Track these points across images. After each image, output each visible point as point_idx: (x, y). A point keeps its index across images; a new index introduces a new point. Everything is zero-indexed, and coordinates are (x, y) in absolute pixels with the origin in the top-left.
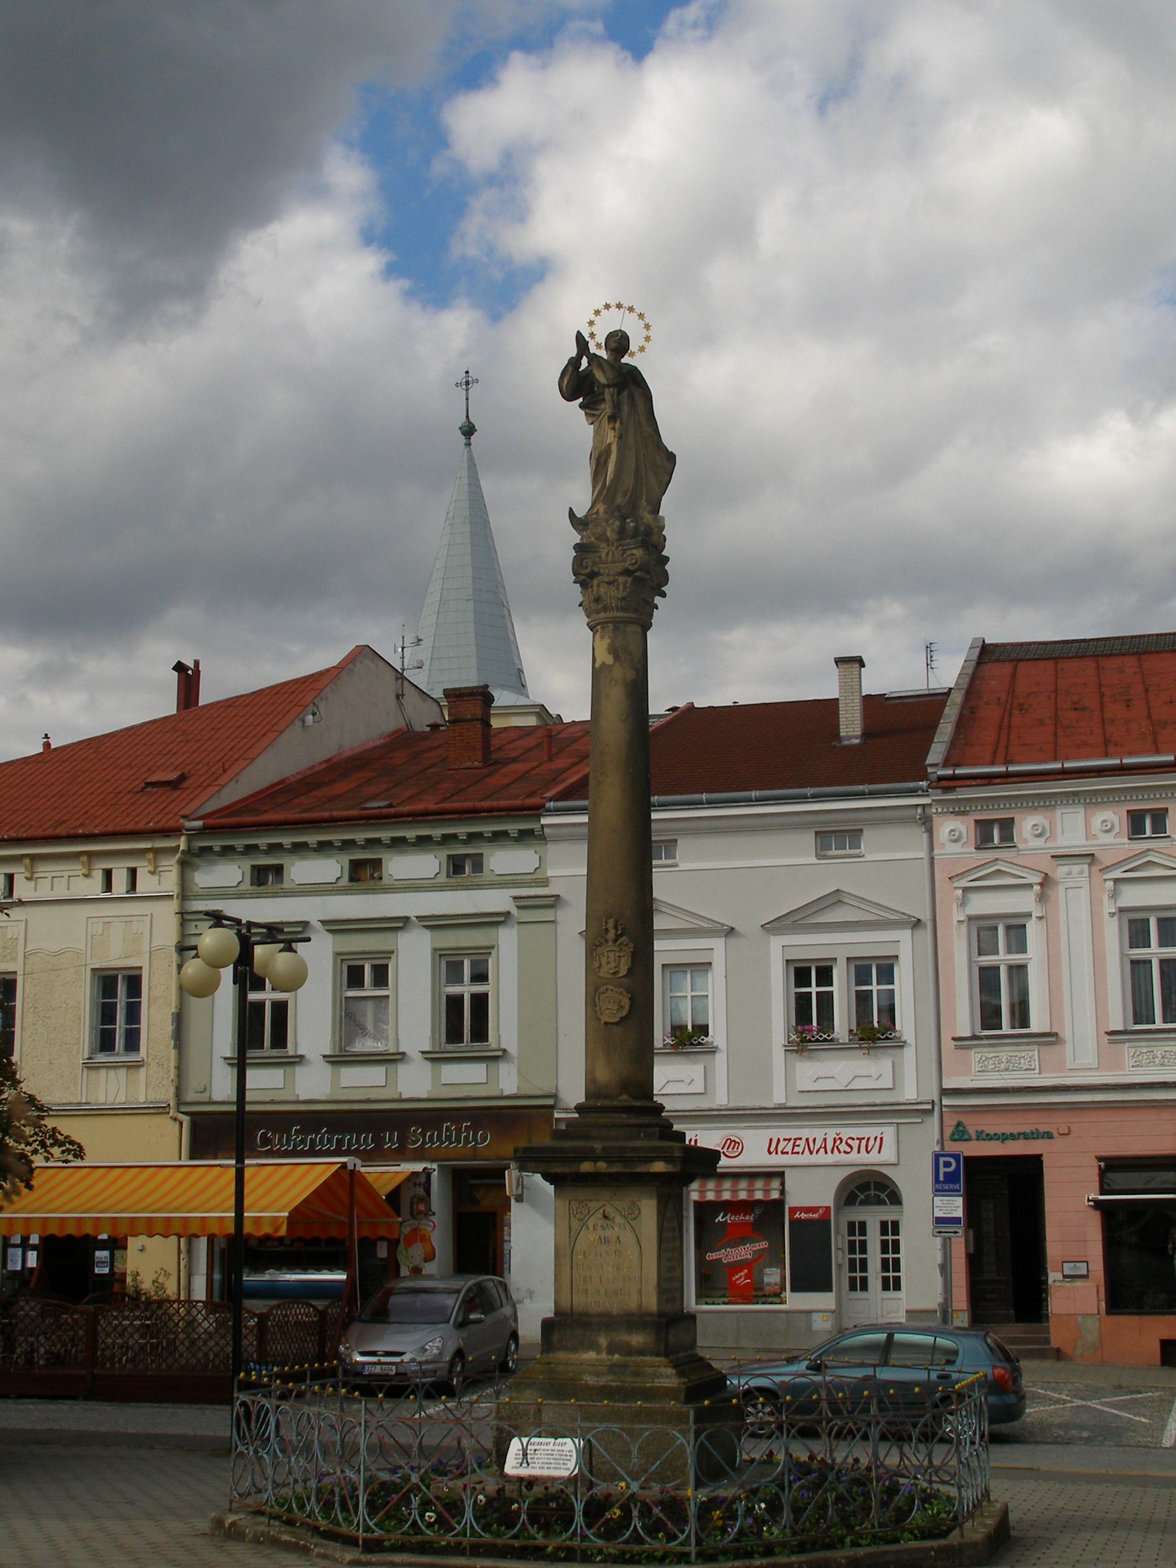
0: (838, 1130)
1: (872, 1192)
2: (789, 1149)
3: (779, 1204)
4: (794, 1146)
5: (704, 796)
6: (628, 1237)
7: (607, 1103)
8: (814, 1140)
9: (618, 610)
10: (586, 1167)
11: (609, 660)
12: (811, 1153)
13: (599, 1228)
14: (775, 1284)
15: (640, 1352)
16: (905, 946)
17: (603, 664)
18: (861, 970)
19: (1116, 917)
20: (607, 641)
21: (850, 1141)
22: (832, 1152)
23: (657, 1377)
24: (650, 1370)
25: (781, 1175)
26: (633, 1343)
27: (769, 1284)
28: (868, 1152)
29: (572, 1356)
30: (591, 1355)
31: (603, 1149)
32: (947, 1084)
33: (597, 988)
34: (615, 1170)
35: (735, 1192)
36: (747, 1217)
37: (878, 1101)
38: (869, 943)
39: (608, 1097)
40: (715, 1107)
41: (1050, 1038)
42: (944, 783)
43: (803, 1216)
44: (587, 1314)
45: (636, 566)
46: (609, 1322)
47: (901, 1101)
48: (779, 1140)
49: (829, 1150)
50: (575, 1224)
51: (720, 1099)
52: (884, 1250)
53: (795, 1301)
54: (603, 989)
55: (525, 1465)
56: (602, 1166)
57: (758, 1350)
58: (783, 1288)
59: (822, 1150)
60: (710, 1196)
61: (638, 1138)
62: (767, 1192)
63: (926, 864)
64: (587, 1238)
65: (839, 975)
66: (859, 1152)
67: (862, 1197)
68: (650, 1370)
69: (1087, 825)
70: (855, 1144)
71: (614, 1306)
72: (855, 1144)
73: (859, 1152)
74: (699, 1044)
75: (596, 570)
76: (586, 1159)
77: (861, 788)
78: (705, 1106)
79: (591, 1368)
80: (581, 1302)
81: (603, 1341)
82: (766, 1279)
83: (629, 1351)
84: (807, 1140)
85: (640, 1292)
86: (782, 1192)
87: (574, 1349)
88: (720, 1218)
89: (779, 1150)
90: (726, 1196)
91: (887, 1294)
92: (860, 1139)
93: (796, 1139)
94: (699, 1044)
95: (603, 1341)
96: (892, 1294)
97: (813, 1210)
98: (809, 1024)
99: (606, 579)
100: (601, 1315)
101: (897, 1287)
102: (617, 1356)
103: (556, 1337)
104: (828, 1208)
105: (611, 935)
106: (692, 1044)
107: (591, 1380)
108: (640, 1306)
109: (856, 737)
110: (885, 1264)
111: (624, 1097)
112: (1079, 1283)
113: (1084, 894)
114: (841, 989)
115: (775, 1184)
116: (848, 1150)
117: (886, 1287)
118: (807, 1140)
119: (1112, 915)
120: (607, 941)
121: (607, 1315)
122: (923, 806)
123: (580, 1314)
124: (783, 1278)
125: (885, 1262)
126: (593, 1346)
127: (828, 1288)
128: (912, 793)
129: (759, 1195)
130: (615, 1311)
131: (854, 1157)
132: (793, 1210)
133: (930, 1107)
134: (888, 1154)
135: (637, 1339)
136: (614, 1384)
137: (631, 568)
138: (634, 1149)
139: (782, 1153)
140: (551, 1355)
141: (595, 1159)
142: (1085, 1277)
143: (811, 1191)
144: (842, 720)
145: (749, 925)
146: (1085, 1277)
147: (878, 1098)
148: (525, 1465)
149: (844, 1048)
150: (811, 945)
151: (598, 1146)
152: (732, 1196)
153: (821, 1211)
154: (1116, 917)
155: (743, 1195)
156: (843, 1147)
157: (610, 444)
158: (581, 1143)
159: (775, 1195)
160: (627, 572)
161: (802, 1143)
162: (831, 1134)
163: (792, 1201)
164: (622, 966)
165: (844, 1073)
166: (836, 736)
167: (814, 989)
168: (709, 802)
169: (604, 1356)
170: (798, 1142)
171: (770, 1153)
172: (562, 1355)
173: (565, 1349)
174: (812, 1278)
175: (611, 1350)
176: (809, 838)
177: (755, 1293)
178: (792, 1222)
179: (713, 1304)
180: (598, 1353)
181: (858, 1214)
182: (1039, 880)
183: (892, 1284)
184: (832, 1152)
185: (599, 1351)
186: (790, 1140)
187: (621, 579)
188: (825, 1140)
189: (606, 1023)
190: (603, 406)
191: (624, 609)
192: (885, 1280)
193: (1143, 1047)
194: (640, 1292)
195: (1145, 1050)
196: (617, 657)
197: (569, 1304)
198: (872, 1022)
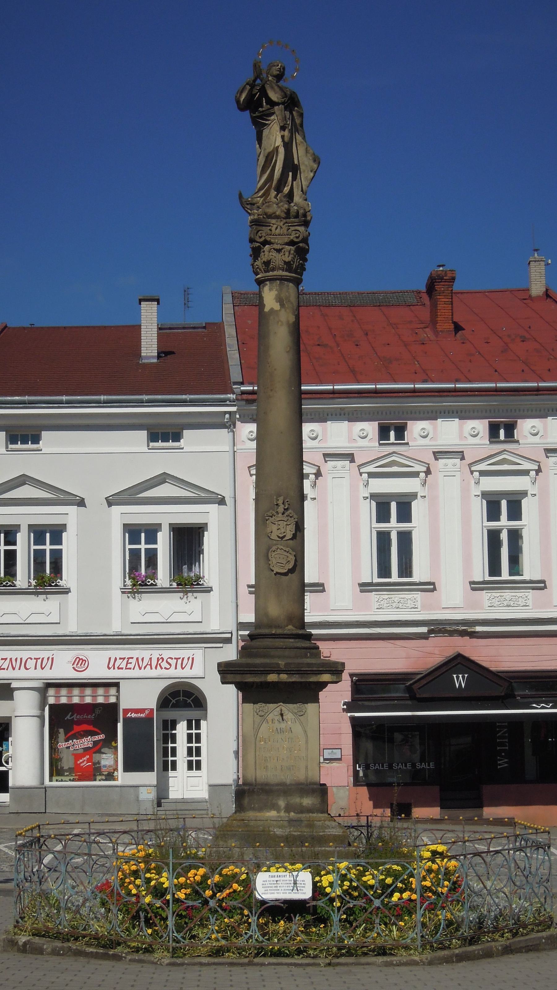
0: (160, 652)
1: (181, 698)
2: (123, 665)
3: (115, 707)
4: (127, 663)
5: (64, 398)
6: (297, 728)
7: (279, 631)
8: (143, 659)
9: (283, 270)
10: (272, 678)
11: (277, 307)
12: (140, 668)
13: (276, 722)
14: (110, 766)
15: (310, 810)
16: (210, 515)
17: (272, 309)
18: (38, 533)
19: (368, 500)
20: (274, 293)
21: (169, 660)
22: (156, 668)
23: (326, 828)
24: (320, 823)
25: (117, 685)
26: (304, 804)
27: (105, 766)
28: (183, 668)
29: (259, 815)
30: (273, 813)
31: (286, 664)
32: (241, 620)
33: (269, 548)
34: (294, 680)
35: (70, 697)
36: (89, 717)
37: (191, 631)
38: (187, 515)
39: (278, 627)
40: (68, 634)
41: (430, 587)
42: (245, 397)
43: (133, 715)
44: (267, 784)
45: (300, 238)
46: (285, 789)
47: (208, 631)
48: (116, 659)
49: (153, 667)
50: (258, 719)
51: (72, 627)
52: (190, 740)
53: (123, 778)
54: (274, 548)
55: (295, 891)
56: (284, 677)
57: (103, 815)
58: (116, 769)
59: (149, 667)
60: (64, 700)
61: (306, 657)
62: (107, 697)
63: (228, 457)
64: (264, 729)
65: (21, 538)
66: (176, 668)
67: (174, 701)
68: (320, 823)
69: (350, 431)
70: (173, 662)
71: (288, 778)
72: (173, 662)
73: (176, 668)
74: (56, 585)
75: (268, 239)
76: (272, 672)
77: (184, 397)
78: (60, 632)
79: (275, 823)
80: (263, 775)
81: (282, 803)
82: (103, 763)
83: (302, 810)
84: (137, 659)
85: (307, 768)
86: (118, 698)
87: (260, 810)
88: (68, 717)
89: (116, 666)
90: (76, 700)
91: (191, 773)
92: (177, 659)
93: (129, 658)
94: (56, 585)
95: (282, 803)
96: (194, 773)
97: (142, 711)
98: (139, 576)
99: (276, 246)
100: (278, 785)
101: (198, 767)
102: (292, 814)
103: (246, 801)
104: (152, 710)
105: (281, 509)
106: (51, 586)
107: (279, 832)
108: (307, 778)
109: (153, 357)
110: (190, 751)
111: (290, 627)
112: (335, 764)
113: (457, 480)
114: (23, 546)
115: (113, 691)
116: (168, 666)
117: (190, 768)
118: (137, 659)
119: (365, 498)
120: (277, 513)
121: (283, 784)
122: (230, 413)
123: (262, 784)
124: (116, 762)
125: (190, 750)
126: (275, 807)
127: (151, 769)
128: (222, 402)
129: (100, 700)
130: (288, 782)
131: (172, 672)
132: (126, 711)
133: (229, 635)
134: (197, 670)
135: (307, 801)
136: (296, 833)
137: (295, 240)
138: (309, 665)
139: (119, 668)
140: (243, 814)
141: (279, 672)
142: (340, 759)
143: (139, 697)
144: (143, 343)
145: (96, 499)
146: (340, 759)
147: (191, 629)
148: (295, 891)
149: (164, 591)
150: (142, 514)
151: (282, 663)
152: (93, 700)
153: (147, 712)
154: (368, 500)
155: (88, 700)
156: (164, 664)
157: (278, 147)
158: (267, 661)
159: (113, 700)
160: (291, 243)
161: (133, 661)
162: (156, 654)
163: (123, 705)
164: (288, 531)
165: (165, 609)
166: (138, 355)
167: (143, 546)
168: (68, 402)
169: (282, 814)
170: (130, 661)
171: (109, 668)
172: (251, 814)
173: (253, 809)
174: (137, 761)
175: (288, 809)
176: (144, 434)
177: (93, 772)
178: (126, 720)
179: (62, 781)
180: (278, 812)
181: (170, 714)
182: (315, 471)
183: (194, 766)
184: (156, 668)
185: (278, 811)
186: (6, 659)
187: (288, 248)
188: (151, 659)
189: (277, 573)
190: (272, 118)
191: (289, 270)
192: (190, 764)
193: (385, 595)
194: (307, 768)
195: (386, 597)
196: (282, 305)
197: (254, 778)
198: (45, 571)
